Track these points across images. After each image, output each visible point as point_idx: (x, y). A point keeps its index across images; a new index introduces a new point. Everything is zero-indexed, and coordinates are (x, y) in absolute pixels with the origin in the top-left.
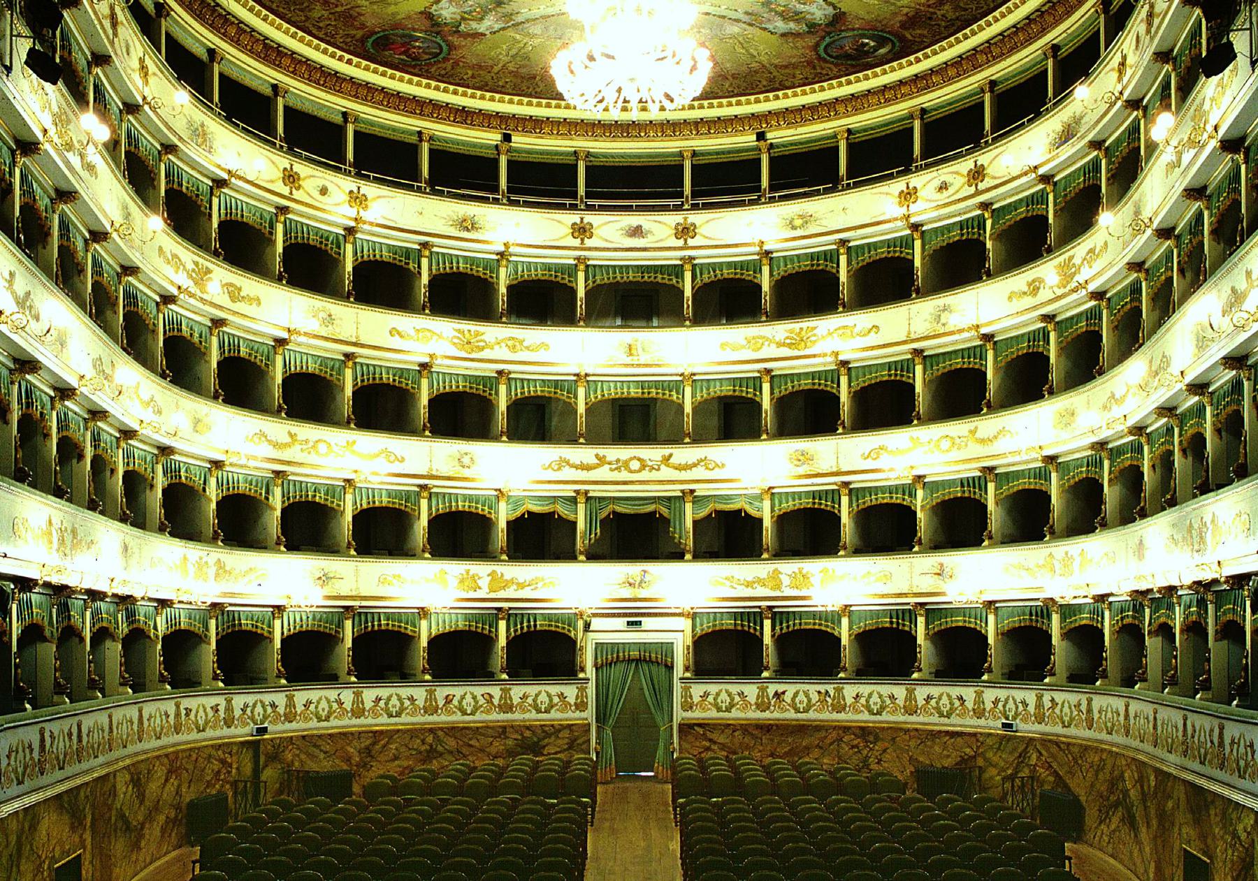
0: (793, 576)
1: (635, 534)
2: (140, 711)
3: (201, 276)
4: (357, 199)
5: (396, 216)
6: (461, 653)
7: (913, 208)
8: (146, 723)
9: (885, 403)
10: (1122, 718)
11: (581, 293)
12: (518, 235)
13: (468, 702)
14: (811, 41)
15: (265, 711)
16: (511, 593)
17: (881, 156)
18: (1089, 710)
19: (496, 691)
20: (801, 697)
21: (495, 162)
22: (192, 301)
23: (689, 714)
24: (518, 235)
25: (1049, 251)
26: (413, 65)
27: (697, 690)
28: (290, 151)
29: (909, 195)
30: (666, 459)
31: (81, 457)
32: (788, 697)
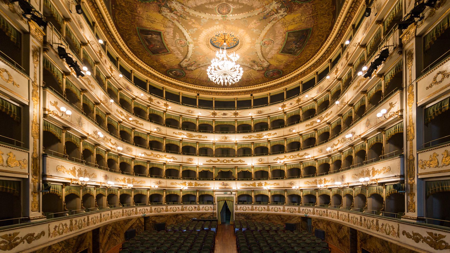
0: (259, 184)
1: (225, 175)
2: (101, 214)
3: (127, 117)
5: (173, 109)
7: (285, 109)
8: (102, 217)
9: (278, 149)
10: (347, 218)
11: (214, 127)
12: (200, 114)
14: (263, 72)
16: (199, 187)
17: (277, 99)
18: (349, 217)
19: (197, 206)
20: (190, 208)
21: (196, 100)
22: (126, 123)
24: (200, 114)
25: (316, 115)
26: (176, 77)
27: (239, 207)
28: (150, 94)
29: (284, 106)
30: (232, 160)
31: (93, 154)
32: (188, 208)
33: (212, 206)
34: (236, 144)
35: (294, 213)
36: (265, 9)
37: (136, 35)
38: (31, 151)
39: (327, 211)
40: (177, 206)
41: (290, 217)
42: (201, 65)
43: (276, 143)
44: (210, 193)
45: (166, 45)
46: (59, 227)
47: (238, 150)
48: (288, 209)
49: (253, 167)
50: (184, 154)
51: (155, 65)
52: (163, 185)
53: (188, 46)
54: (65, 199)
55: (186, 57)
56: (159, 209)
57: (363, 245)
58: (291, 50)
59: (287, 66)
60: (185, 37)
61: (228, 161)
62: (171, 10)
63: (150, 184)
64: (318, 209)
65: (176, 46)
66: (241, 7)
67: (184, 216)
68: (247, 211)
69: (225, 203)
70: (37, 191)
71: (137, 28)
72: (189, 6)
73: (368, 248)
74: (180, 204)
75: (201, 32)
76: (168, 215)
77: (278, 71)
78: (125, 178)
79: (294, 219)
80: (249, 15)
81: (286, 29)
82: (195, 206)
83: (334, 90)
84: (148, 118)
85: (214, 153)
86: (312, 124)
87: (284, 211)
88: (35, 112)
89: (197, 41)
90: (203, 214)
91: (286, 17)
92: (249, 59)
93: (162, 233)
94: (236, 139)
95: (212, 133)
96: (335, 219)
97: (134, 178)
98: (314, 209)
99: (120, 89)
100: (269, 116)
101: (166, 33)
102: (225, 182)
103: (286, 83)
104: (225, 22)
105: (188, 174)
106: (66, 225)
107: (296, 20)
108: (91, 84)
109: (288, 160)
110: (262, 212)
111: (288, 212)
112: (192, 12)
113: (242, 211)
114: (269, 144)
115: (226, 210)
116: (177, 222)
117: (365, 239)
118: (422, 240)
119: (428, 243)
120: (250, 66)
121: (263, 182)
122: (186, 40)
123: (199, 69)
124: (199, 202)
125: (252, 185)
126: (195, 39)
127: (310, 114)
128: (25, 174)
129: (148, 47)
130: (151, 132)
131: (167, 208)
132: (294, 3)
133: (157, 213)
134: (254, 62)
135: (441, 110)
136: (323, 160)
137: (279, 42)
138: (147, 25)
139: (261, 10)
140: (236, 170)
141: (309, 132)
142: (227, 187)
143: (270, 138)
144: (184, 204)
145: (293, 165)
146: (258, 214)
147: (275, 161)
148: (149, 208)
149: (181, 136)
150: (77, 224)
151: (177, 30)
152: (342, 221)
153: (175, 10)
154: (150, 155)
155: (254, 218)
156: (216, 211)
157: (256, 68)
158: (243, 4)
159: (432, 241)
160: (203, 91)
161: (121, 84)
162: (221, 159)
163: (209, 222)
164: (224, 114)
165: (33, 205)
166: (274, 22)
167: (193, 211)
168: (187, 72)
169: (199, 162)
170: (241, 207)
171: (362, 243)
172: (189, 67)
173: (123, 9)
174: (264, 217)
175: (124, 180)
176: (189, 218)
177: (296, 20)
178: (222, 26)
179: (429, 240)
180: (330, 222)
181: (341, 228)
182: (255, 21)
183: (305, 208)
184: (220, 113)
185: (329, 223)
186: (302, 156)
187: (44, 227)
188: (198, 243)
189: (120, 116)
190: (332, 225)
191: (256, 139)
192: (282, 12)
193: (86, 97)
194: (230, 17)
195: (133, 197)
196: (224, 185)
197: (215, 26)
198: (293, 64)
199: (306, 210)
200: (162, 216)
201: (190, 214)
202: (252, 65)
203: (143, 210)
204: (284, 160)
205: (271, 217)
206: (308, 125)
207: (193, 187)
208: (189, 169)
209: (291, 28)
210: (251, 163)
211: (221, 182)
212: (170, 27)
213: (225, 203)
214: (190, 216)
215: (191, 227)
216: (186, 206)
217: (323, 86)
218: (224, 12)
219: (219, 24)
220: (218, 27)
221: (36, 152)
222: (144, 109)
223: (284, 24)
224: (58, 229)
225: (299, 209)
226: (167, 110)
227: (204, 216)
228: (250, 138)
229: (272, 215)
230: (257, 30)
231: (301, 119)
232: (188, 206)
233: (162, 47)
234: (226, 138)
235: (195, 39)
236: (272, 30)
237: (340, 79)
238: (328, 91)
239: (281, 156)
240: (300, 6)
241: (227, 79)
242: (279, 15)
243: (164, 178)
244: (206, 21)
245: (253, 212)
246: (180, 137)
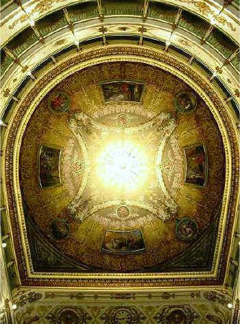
138: (194, 191)
166: (77, 198)
209: (59, 190)
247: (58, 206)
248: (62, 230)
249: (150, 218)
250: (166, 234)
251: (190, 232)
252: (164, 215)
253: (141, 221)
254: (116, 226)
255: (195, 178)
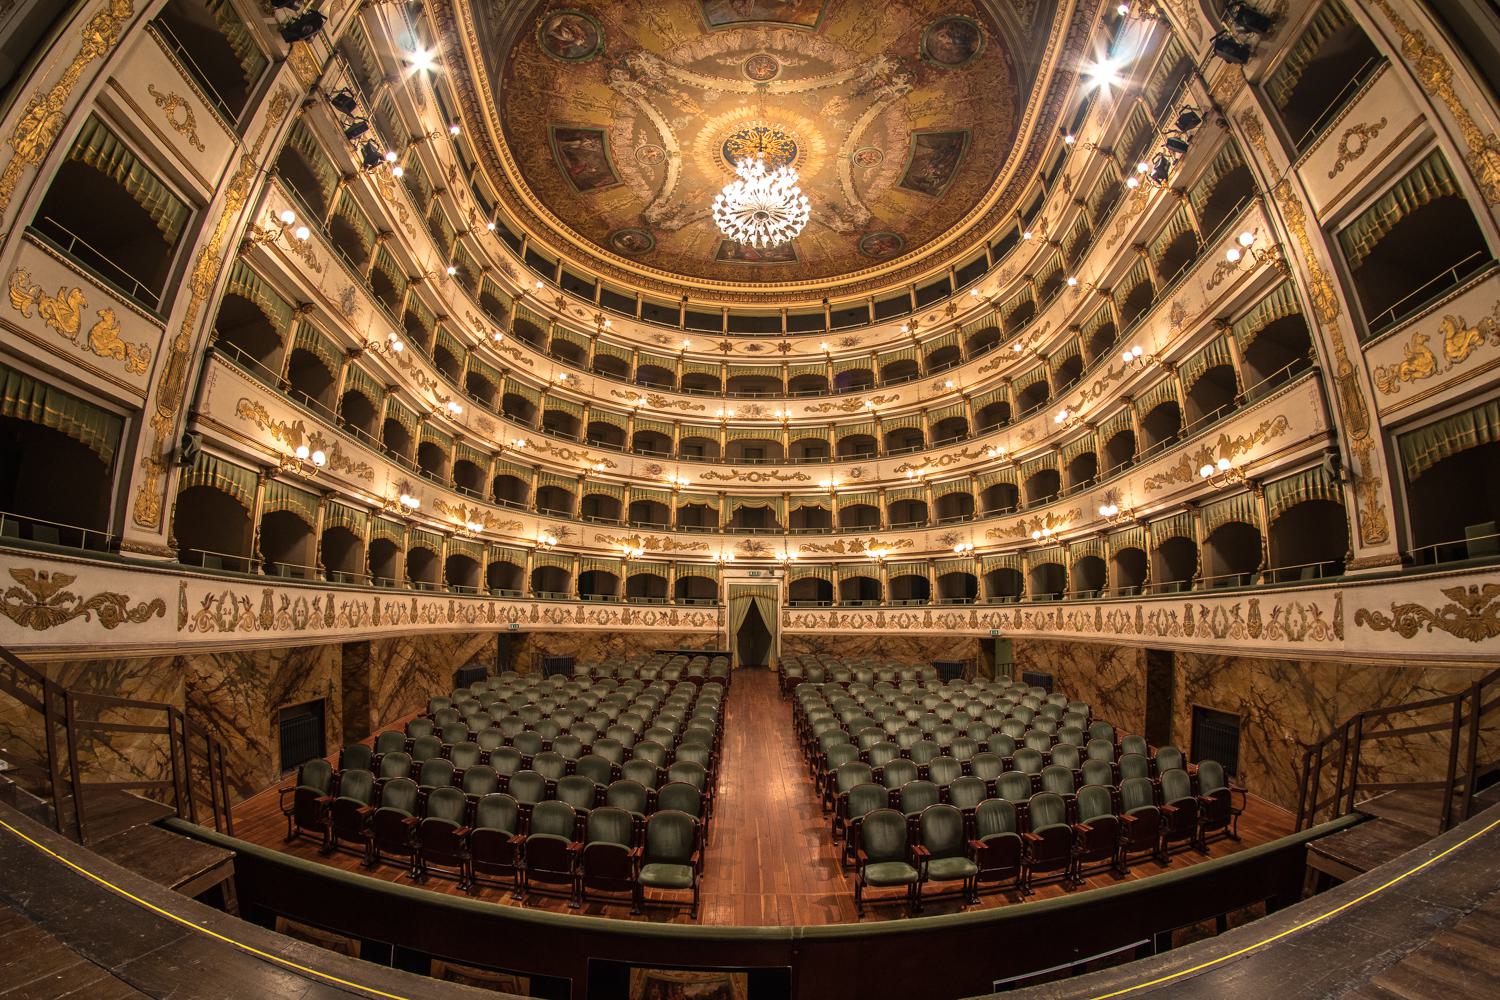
0: (852, 544)
1: (754, 519)
4: (599, 319)
5: (620, 331)
6: (646, 587)
13: (650, 619)
14: (855, 238)
15: (1304, 619)
16: (679, 551)
19: (668, 611)
20: (650, 615)
21: (679, 311)
23: (788, 629)
26: (633, 253)
27: (793, 615)
29: (913, 325)
30: (774, 474)
32: (641, 616)
33: (714, 613)
34: (786, 427)
35: (958, 630)
36: (860, 72)
37: (546, 144)
38: (173, 326)
39: (1060, 611)
40: (610, 609)
41: (946, 642)
42: (698, 215)
43: (898, 425)
44: (709, 574)
45: (612, 164)
46: (222, 602)
47: (792, 445)
48: (940, 618)
49: (834, 494)
50: (636, 452)
51: (582, 220)
52: (573, 540)
53: (667, 163)
54: (263, 526)
55: (659, 194)
56: (558, 612)
57: (1201, 694)
58: (923, 180)
59: (915, 224)
60: (661, 138)
61: (764, 477)
62: (634, 75)
63: (534, 534)
64: (1030, 610)
65: (637, 165)
66: (802, 63)
67: (630, 639)
68: (817, 629)
69: (754, 608)
70: (166, 461)
71: (548, 126)
72: (678, 61)
73: (1218, 700)
74: (618, 603)
75: (703, 124)
76: (582, 634)
77: (894, 238)
78: (464, 507)
79: (957, 648)
80: (821, 84)
81: (910, 126)
82: (663, 610)
83: (1041, 275)
84: (548, 349)
85: (722, 454)
86: (995, 364)
87: (928, 624)
88: (221, 231)
89: (690, 148)
90: (685, 636)
91: (911, 96)
92: (822, 198)
93: (558, 682)
94: (785, 413)
95: (719, 395)
96: (1089, 634)
97: (492, 511)
98: (1018, 612)
99: (487, 268)
100: (874, 352)
101: (616, 132)
102: (754, 540)
103: (913, 271)
104: (763, 97)
105: (648, 513)
106: (246, 601)
107: (934, 106)
108: (408, 221)
109: (935, 469)
110: (864, 630)
111: (940, 627)
112: (684, 76)
113: (803, 629)
114: (879, 428)
115: (754, 630)
116: (609, 655)
117: (1207, 675)
118: (1426, 623)
119: (1447, 626)
120: (822, 220)
121: (865, 538)
122: (664, 147)
123: (691, 227)
124: (675, 598)
125: (832, 548)
126: (686, 143)
127: (985, 341)
128: (134, 390)
129: (569, 171)
130: (551, 383)
131: (580, 612)
132: (928, 65)
133: (550, 626)
134: (833, 207)
135: (1382, 224)
136: (1036, 462)
137: (896, 156)
138: (573, 116)
139: (850, 73)
140: (787, 503)
141: (990, 386)
142: (760, 554)
143: (882, 408)
144: (631, 602)
145: (949, 485)
146: (850, 638)
147: (900, 475)
148: (528, 607)
149: (634, 401)
150: (290, 611)
151: (643, 122)
152: (1112, 635)
153: (644, 73)
154: (541, 450)
155: (839, 648)
156: (725, 629)
157: (839, 225)
158: (808, 57)
159: (1459, 613)
160: (699, 291)
161: (492, 255)
162: (744, 470)
163: (705, 659)
164: (754, 348)
165: (143, 505)
166: (882, 104)
167: (656, 627)
168: (659, 236)
169: (680, 478)
170: (799, 617)
171: (1195, 687)
172: (665, 220)
173: (526, 84)
174: (868, 645)
175: (461, 511)
176: (646, 648)
177: (934, 106)
178: (754, 107)
179: (1451, 617)
180: (1072, 643)
181: (1112, 655)
182: (836, 99)
183: (989, 612)
184: (740, 346)
185: (1066, 648)
186: (976, 455)
187: (164, 587)
188: (667, 719)
189: (474, 330)
190: (1079, 654)
191: (842, 412)
192: (900, 82)
193: (388, 254)
194: (777, 86)
195: (485, 568)
196: (749, 548)
197: (738, 110)
198: (930, 222)
199: (996, 618)
200: (564, 635)
201: (649, 634)
202: (828, 218)
203: (512, 612)
204: (926, 471)
205: (890, 645)
206: (986, 369)
207: (660, 551)
208: (650, 497)
209: (923, 123)
210: (830, 480)
211: (742, 539)
212: (626, 116)
213: (754, 608)
214: (648, 642)
215: (649, 670)
216: (637, 609)
217: (1013, 267)
218: (763, 73)
219: (748, 105)
220: (745, 112)
221: (188, 336)
222: (540, 325)
223: (907, 113)
224: (219, 608)
225: (974, 616)
226: (600, 330)
227: (688, 642)
228: (826, 410)
229: (893, 638)
230: (843, 121)
231: (963, 354)
232: (643, 610)
233: (602, 170)
234: (758, 410)
235: (686, 143)
236: (879, 125)
237: (1055, 243)
238: (1028, 277)
239: (918, 459)
240: (942, 73)
241: (766, 232)
242: (894, 89)
243: (575, 520)
244: (715, 96)
245: (835, 630)
246: (630, 404)
247: (940, 93)
248: (945, 41)
249: (684, 55)
250: (631, 21)
251: (559, 30)
252: (645, 63)
253: (710, 48)
254: (781, 38)
255: (580, 139)
